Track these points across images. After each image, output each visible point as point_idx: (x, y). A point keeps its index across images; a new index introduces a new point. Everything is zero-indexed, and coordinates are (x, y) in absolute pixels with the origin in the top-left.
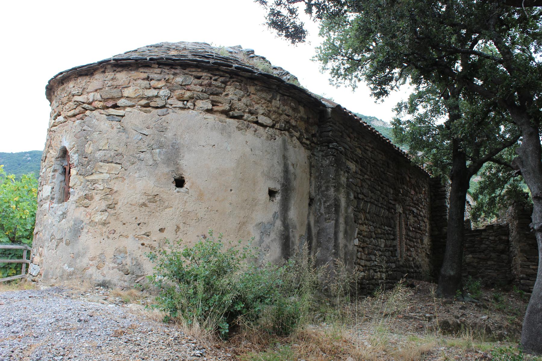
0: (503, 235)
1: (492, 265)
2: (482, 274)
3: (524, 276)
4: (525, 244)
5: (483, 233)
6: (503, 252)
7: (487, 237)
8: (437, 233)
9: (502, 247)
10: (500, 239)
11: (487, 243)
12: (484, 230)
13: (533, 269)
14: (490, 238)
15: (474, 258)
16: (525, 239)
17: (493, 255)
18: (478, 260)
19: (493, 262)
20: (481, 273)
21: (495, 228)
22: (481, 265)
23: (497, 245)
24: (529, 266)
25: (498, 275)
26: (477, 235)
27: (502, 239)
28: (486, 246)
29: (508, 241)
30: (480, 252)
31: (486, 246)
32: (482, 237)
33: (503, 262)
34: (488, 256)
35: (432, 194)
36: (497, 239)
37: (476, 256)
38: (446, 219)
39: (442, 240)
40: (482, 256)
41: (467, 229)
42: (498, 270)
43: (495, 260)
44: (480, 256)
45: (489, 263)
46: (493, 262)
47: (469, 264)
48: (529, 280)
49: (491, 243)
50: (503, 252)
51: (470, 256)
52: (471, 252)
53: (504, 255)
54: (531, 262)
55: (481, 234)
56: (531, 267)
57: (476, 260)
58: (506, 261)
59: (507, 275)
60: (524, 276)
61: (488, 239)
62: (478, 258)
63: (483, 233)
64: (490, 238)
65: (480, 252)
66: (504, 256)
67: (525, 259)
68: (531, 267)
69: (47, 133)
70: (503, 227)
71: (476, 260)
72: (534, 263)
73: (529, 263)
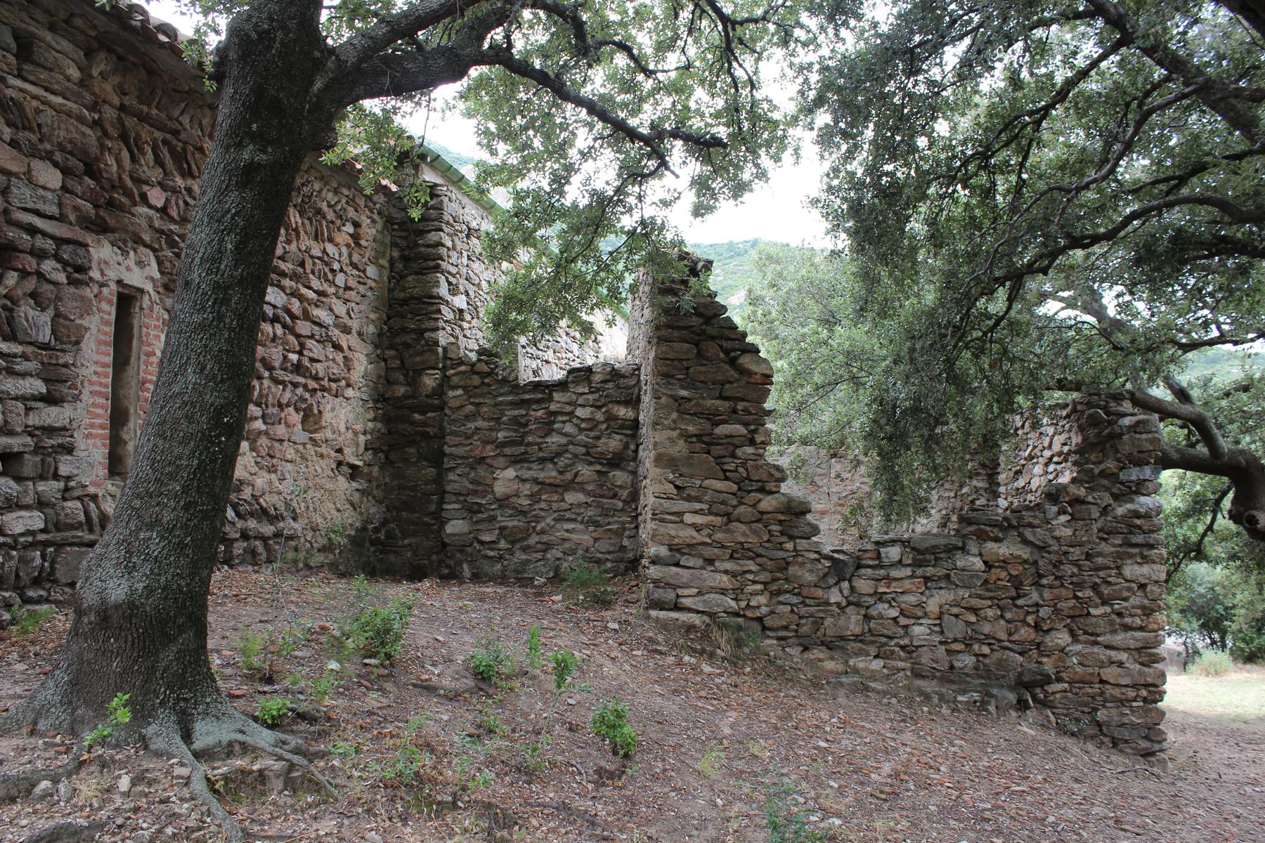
0: (619, 403)
1: (580, 505)
2: (545, 538)
3: (664, 551)
4: (675, 434)
5: (556, 396)
6: (616, 461)
7: (568, 409)
8: (401, 390)
9: (613, 443)
10: (610, 418)
11: (569, 428)
12: (562, 385)
13: (694, 525)
14: (580, 412)
15: (523, 481)
16: (675, 415)
17: (586, 471)
18: (536, 488)
19: (581, 497)
20: (543, 532)
21: (597, 378)
22: (543, 505)
23: (598, 438)
24: (680, 514)
25: (596, 540)
26: (538, 401)
27: (616, 418)
28: (564, 440)
29: (636, 421)
30: (542, 460)
31: (564, 440)
32: (553, 407)
33: (615, 496)
34: (569, 476)
35: (396, 254)
36: (599, 416)
37: (528, 474)
38: (436, 343)
39: (417, 416)
40: (549, 473)
41: (505, 381)
42: (597, 524)
43: (590, 488)
44: (542, 475)
45: (571, 497)
46: (581, 497)
47: (503, 502)
48: (677, 565)
49: (581, 430)
50: (616, 461)
51: (510, 473)
52: (516, 461)
53: (618, 473)
54: (689, 499)
55: (550, 399)
56: (689, 518)
57: (526, 489)
58: (624, 494)
59: (626, 542)
60: (664, 551)
61: (571, 414)
62: (536, 481)
63: (556, 396)
64: (580, 412)
65: (542, 460)
66: (620, 477)
67: (670, 489)
68: (689, 518)
69: (773, 240)
70: (624, 376)
71: (526, 489)
72: (698, 506)
73: (681, 505)
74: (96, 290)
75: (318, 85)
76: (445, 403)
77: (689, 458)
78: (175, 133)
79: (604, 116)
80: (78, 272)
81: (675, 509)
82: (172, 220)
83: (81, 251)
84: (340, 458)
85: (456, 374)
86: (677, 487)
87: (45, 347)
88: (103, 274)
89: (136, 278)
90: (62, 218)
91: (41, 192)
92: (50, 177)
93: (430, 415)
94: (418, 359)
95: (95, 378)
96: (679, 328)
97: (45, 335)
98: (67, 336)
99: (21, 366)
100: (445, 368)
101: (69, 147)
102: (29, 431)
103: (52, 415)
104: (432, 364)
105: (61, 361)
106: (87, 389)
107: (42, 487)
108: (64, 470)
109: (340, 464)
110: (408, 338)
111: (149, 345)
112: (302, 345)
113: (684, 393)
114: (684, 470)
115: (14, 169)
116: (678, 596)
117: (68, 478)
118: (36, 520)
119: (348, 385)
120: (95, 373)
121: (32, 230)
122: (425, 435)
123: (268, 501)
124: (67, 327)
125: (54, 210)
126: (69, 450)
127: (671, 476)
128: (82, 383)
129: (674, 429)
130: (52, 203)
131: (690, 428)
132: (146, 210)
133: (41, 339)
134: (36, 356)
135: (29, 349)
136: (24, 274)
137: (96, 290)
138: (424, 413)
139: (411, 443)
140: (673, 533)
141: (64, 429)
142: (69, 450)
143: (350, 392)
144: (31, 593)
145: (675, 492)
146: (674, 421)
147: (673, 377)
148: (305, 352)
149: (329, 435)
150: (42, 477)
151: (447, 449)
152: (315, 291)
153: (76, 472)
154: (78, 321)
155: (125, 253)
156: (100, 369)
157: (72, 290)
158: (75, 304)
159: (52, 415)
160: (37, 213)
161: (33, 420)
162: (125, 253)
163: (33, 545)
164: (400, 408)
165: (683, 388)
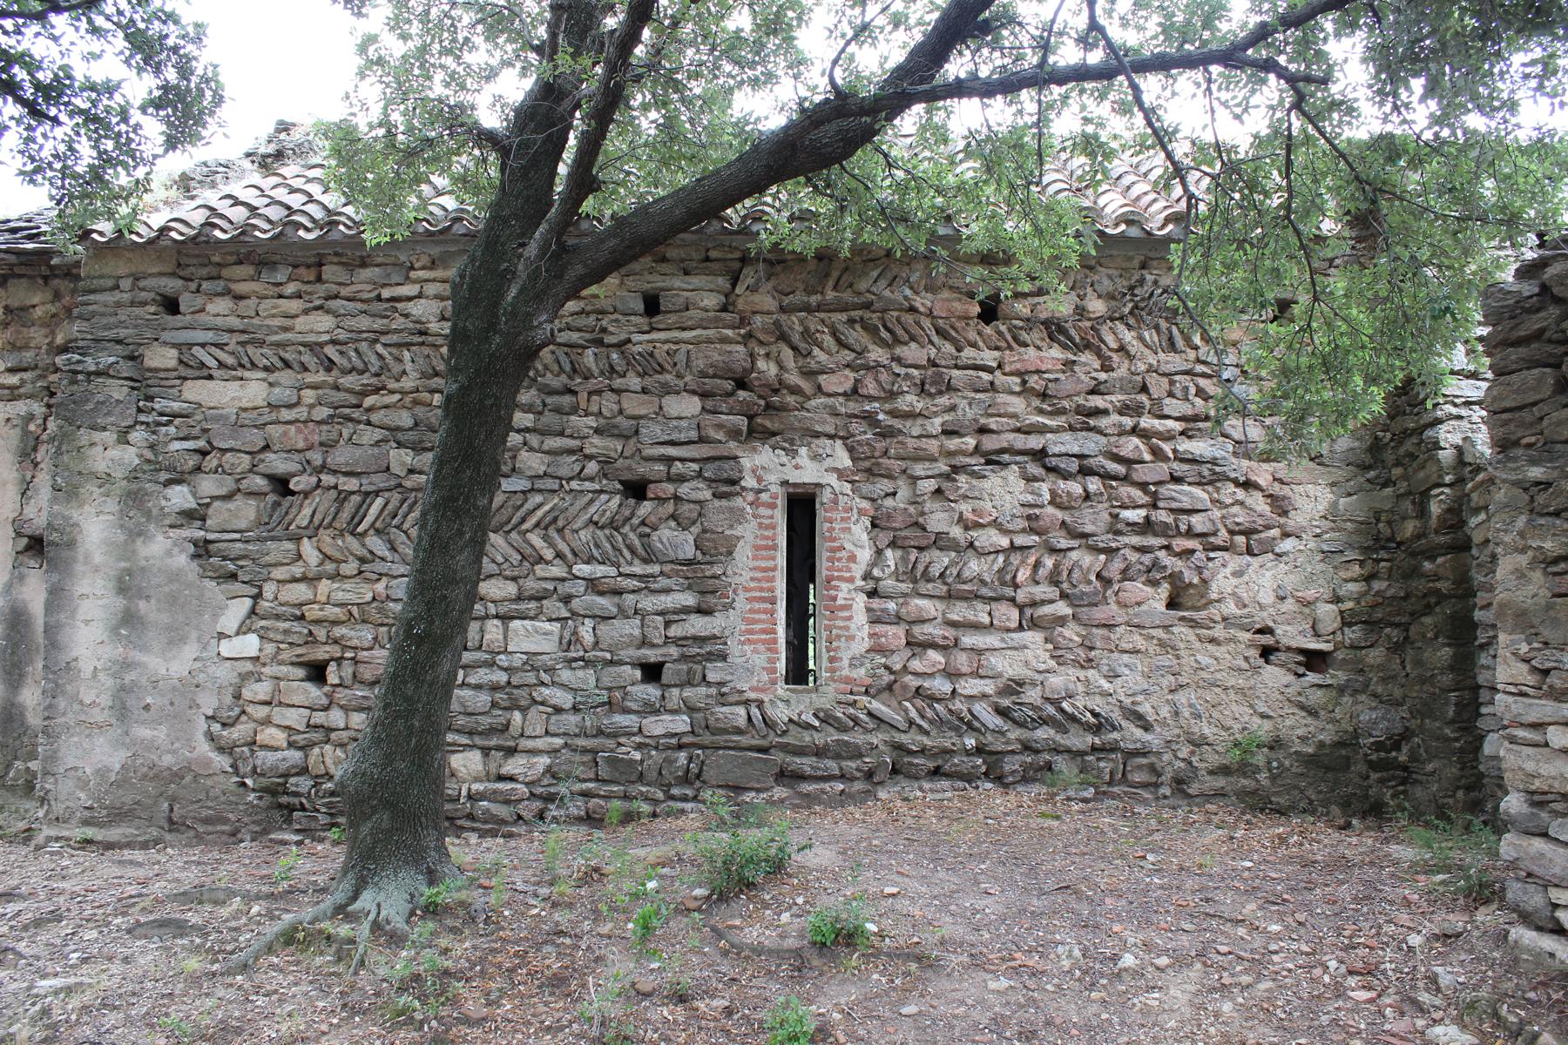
39: (1427, 565)
73: (1544, 709)
74: (750, 497)
75: (513, 292)
76: (1469, 539)
77: (1549, 607)
78: (867, 306)
79: (1189, 62)
80: (727, 486)
81: (1532, 718)
82: (871, 398)
83: (726, 465)
84: (1266, 640)
85: (1474, 489)
86: (1534, 670)
87: (689, 563)
88: (760, 480)
89: (806, 471)
90: (702, 440)
91: (675, 423)
92: (689, 406)
93: (1440, 560)
94: (1421, 474)
95: (752, 585)
96: (1517, 343)
97: (689, 551)
98: (714, 548)
99: (663, 582)
100: (1460, 481)
101: (711, 371)
102: (678, 641)
103: (697, 625)
104: (1434, 479)
105: (708, 573)
106: (742, 595)
107: (688, 692)
108: (712, 677)
109: (1266, 652)
110: (1409, 445)
111: (834, 540)
112: (1155, 495)
113: (1536, 473)
114: (1547, 633)
115: (643, 412)
116: (1556, 906)
117: (721, 684)
118: (681, 723)
119: (1286, 535)
120: (752, 579)
121: (669, 460)
122: (1441, 597)
123: (1078, 704)
124: (714, 540)
125: (693, 435)
126: (723, 657)
127: (1524, 648)
128: (735, 591)
129: (1523, 551)
130: (689, 429)
131: (1548, 545)
132: (823, 400)
133: (681, 556)
134: (677, 573)
135: (667, 568)
136: (661, 500)
137: (750, 497)
138: (1432, 558)
139: (1428, 610)
140: (1530, 766)
141: (715, 637)
142: (723, 657)
143: (1288, 545)
144: (675, 791)
145: (1531, 679)
146: (1521, 534)
147: (1516, 443)
148: (1161, 504)
149: (1230, 608)
150: (690, 683)
151: (1478, 615)
152: (1177, 419)
153: (729, 678)
154: (728, 532)
155: (792, 453)
156: (759, 575)
157: (717, 503)
158: (722, 516)
159: (697, 625)
160: (672, 443)
161: (674, 631)
162: (792, 453)
163: (680, 747)
164: (1413, 554)
165: (1533, 462)
